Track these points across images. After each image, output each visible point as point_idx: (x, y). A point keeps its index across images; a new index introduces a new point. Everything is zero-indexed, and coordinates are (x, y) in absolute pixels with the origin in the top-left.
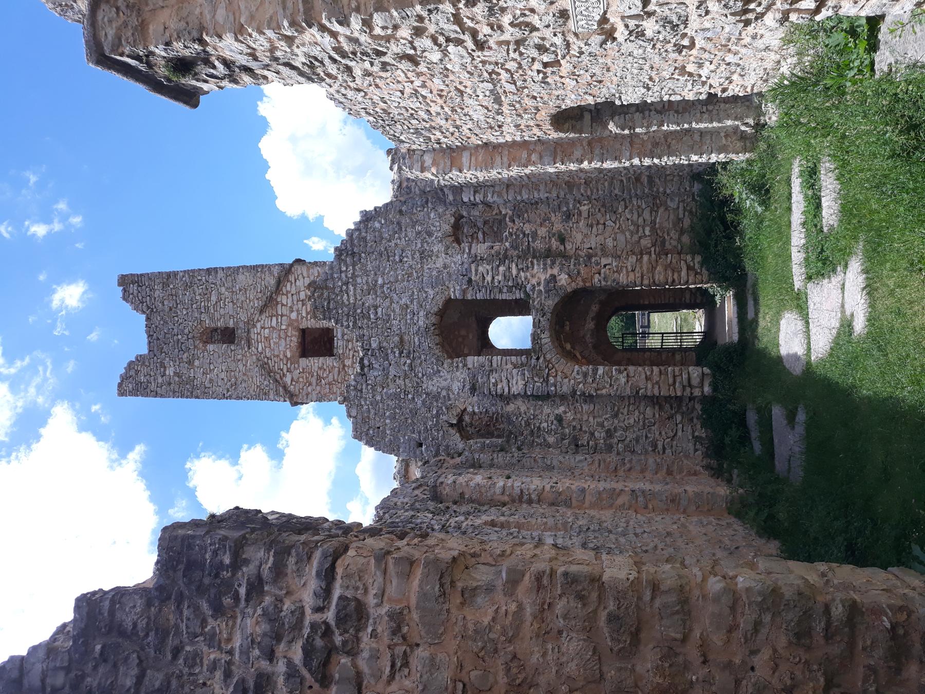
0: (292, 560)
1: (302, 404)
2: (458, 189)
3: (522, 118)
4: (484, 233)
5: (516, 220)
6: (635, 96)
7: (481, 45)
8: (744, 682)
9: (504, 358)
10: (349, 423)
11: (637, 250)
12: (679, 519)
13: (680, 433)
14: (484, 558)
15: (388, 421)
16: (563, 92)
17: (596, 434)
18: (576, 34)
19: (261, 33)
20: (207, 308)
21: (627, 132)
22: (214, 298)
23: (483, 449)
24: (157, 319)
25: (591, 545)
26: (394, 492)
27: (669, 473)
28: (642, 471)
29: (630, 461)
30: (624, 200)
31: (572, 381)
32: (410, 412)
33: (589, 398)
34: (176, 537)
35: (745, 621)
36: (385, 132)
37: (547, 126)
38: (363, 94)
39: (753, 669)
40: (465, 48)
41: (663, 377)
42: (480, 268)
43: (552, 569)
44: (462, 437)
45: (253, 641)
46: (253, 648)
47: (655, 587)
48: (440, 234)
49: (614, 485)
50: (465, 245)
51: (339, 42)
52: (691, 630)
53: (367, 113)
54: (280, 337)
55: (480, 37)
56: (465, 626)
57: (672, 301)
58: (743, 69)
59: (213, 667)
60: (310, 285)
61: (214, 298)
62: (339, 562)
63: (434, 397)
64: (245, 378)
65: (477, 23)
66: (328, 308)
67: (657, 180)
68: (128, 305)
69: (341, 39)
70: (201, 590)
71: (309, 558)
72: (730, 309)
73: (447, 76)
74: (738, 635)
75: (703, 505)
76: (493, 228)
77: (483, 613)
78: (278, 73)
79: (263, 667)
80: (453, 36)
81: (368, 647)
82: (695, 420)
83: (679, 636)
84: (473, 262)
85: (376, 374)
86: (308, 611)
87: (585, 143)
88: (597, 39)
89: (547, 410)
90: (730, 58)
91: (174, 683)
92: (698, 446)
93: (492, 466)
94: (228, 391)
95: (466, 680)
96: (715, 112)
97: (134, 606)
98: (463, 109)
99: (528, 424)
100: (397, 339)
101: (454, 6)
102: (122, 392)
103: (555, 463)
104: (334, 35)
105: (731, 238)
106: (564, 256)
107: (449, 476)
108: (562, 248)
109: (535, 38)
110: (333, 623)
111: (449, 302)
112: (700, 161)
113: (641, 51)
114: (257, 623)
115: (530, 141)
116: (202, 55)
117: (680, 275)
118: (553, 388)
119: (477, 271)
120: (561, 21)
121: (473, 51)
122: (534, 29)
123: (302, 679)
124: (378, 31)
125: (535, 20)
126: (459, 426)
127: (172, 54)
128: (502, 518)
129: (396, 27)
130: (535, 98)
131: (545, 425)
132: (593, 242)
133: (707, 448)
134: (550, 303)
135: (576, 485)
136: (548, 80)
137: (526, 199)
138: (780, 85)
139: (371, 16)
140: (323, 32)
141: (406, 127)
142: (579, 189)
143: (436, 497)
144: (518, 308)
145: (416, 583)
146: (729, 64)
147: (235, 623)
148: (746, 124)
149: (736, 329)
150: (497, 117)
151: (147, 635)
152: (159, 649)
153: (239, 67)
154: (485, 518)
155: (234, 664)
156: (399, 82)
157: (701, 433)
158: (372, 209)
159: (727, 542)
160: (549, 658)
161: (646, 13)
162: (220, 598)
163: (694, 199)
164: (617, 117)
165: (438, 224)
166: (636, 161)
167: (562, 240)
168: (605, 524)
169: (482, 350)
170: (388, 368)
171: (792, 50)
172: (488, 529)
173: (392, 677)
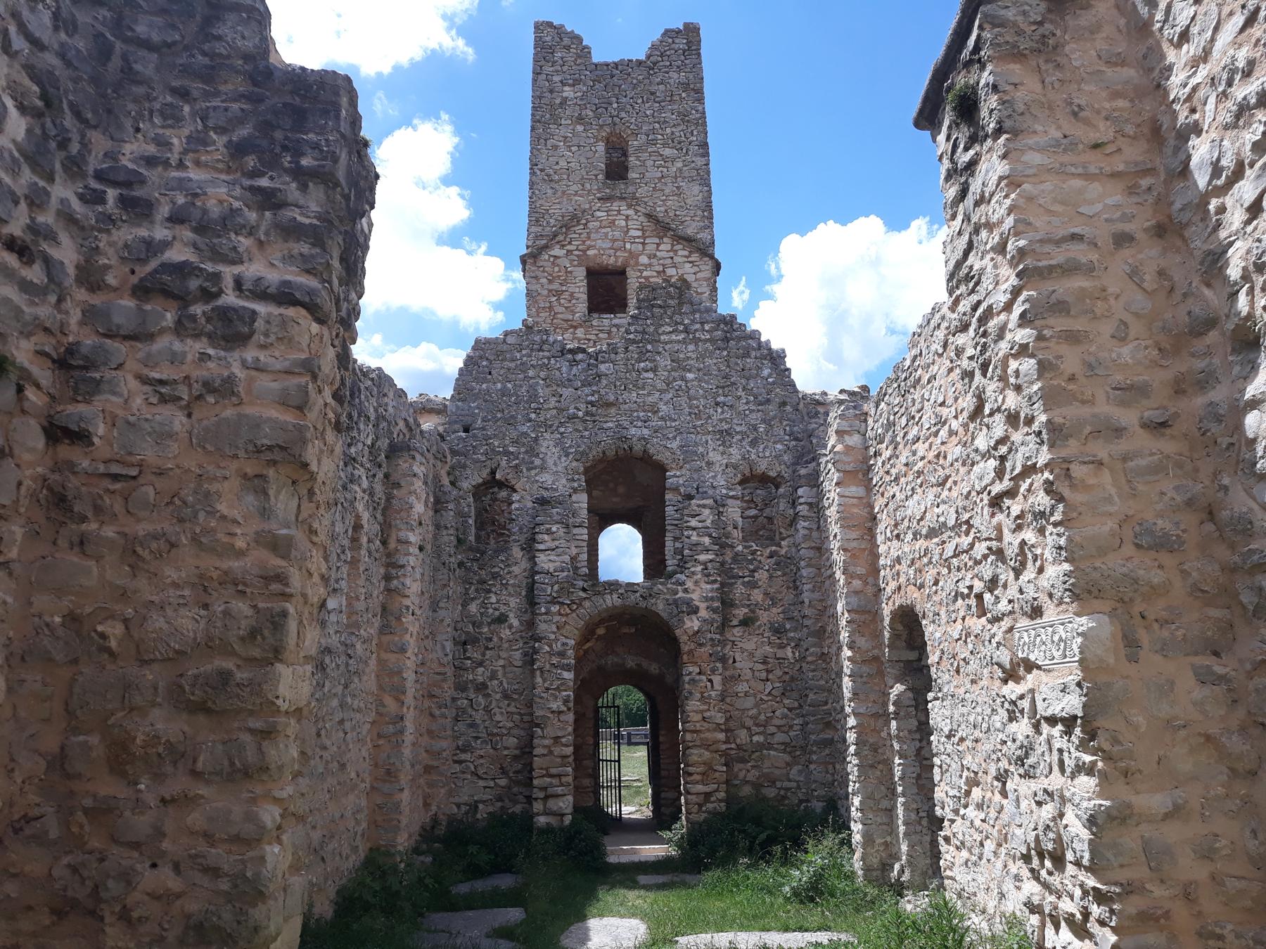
0: (305, 248)
1: (524, 271)
2: (814, 481)
3: (910, 566)
4: (756, 517)
5: (773, 560)
6: (939, 719)
7: (996, 503)
8: (136, 854)
9: (585, 544)
10: (498, 334)
11: (732, 724)
12: (363, 781)
13: (482, 783)
14: (307, 508)
15: (499, 386)
16: (944, 620)
17: (481, 670)
18: (1011, 629)
19: (1010, 210)
20: (653, 142)
21: (891, 708)
22: (667, 152)
23: (460, 514)
24: (639, 75)
25: (327, 660)
26: (401, 394)
27: (428, 769)
28: (430, 732)
29: (444, 716)
30: (801, 706)
31: (553, 637)
32: (512, 417)
33: (530, 659)
34: (337, 94)
35: (218, 855)
36: (890, 382)
37: (899, 601)
38: (940, 351)
39: (154, 866)
40: (993, 482)
41: (559, 760)
42: (707, 512)
43: (292, 595)
44: (477, 487)
45: (196, 195)
46: (186, 196)
47: (268, 734)
48: (753, 457)
49: (410, 692)
50: (738, 491)
51: (999, 314)
52: (208, 782)
53: (915, 357)
54: (614, 241)
55: (1007, 502)
56: (215, 478)
57: (663, 776)
58: (975, 864)
59: (163, 143)
60: (685, 281)
61: (667, 152)
62: (303, 312)
63: (532, 449)
64: (559, 193)
65: (1025, 497)
66: (653, 306)
67: (827, 751)
68: (659, 37)
69: (1003, 317)
70: (266, 127)
71: (308, 272)
72: (652, 851)
73: (964, 464)
74: (202, 846)
75: (383, 815)
76: (763, 529)
77: (232, 503)
78: (960, 233)
79: (161, 209)
80: (1008, 465)
81: (187, 349)
82: (499, 804)
83: (199, 766)
84: (716, 502)
85: (564, 369)
86: (237, 269)
87: (876, 651)
88: (1004, 657)
89: (514, 602)
90: (990, 846)
91: (140, 90)
92: (464, 809)
93: (438, 527)
94: (541, 170)
95: (141, 480)
96: (919, 828)
97: (243, 38)
98: (921, 486)
99: (495, 576)
100: (612, 398)
101: (1046, 465)
102: (538, 27)
103: (442, 613)
104: (1008, 307)
105: (750, 852)
106: (725, 625)
107: (423, 468)
108: (735, 622)
109: (1006, 575)
110: (220, 302)
111: (661, 469)
112: (853, 809)
113: (998, 725)
114: (221, 202)
115: (878, 578)
116: (981, 133)
117: (697, 783)
118: (543, 610)
119: (704, 506)
120: (1028, 609)
121: (989, 493)
122: (1018, 573)
123: (143, 261)
124: (1013, 365)
125: (1030, 573)
126: (493, 483)
127: (982, 94)
128: (364, 540)
129: (1018, 388)
130: (936, 583)
131: (493, 600)
132: (743, 664)
133: (462, 820)
134: (660, 607)
135: (411, 642)
136: (960, 601)
137: (802, 573)
138: (951, 912)
139: (1032, 356)
140: (1011, 293)
141: (896, 409)
142: (814, 645)
143: (395, 450)
144: (654, 562)
145: (274, 413)
146: (982, 844)
147: (221, 171)
148: (902, 871)
149: (624, 859)
150: (910, 532)
151: (205, 54)
152: (186, 71)
153: (966, 182)
154: (366, 516)
155: (165, 169)
156: (956, 399)
157: (483, 812)
158: (788, 366)
159: (331, 847)
160: (171, 592)
161: (1039, 722)
162: (254, 152)
163: (801, 801)
164: (911, 695)
165: (767, 454)
166: (852, 722)
167: (745, 623)
168: (356, 680)
169: (597, 514)
170: (571, 386)
171: (999, 928)
172: (350, 520)
173: (145, 381)
